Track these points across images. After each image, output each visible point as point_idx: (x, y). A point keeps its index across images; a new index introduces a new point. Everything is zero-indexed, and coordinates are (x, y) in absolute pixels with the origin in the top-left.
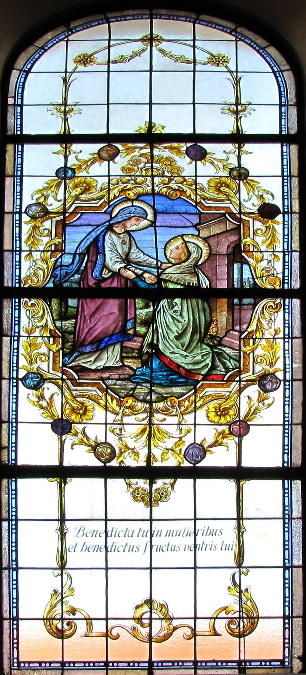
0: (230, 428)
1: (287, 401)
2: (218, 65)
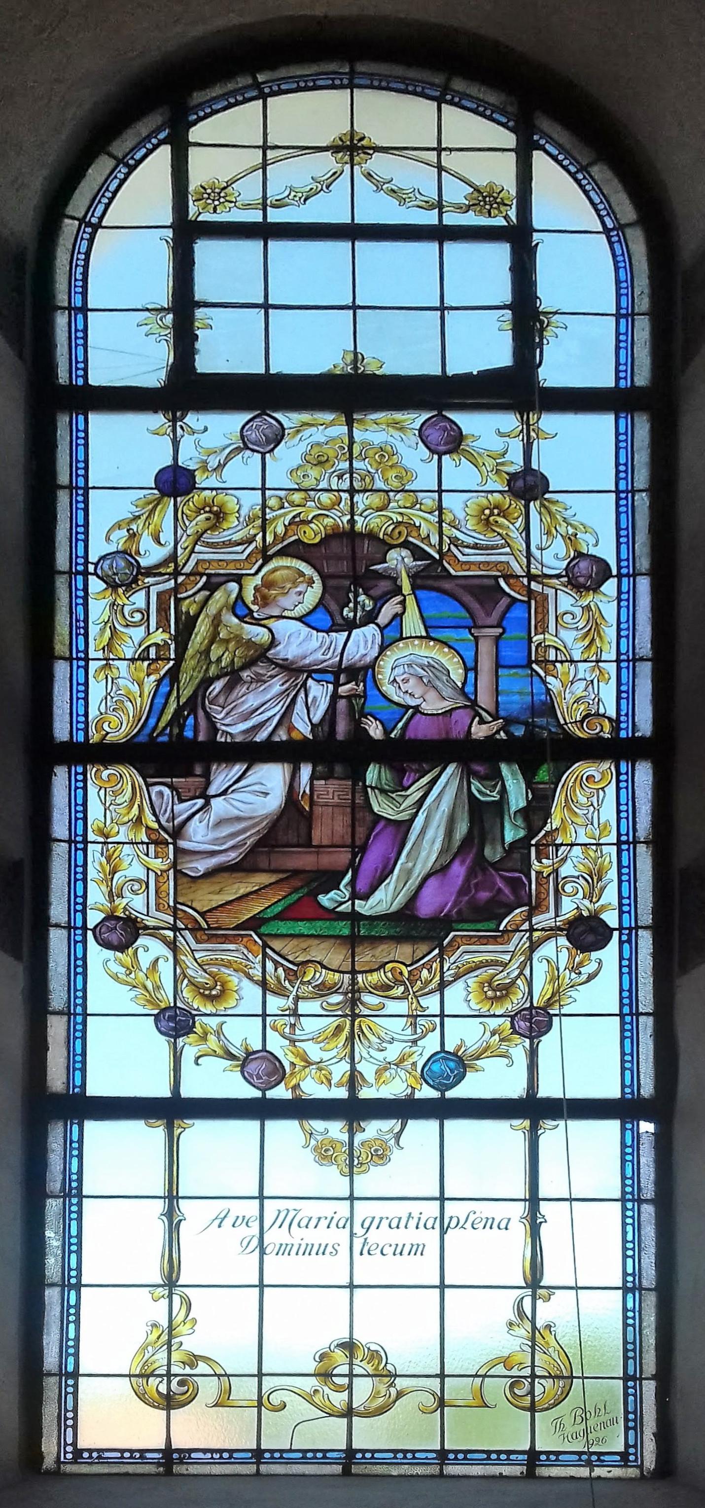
0: (512, 1023)
1: (628, 967)
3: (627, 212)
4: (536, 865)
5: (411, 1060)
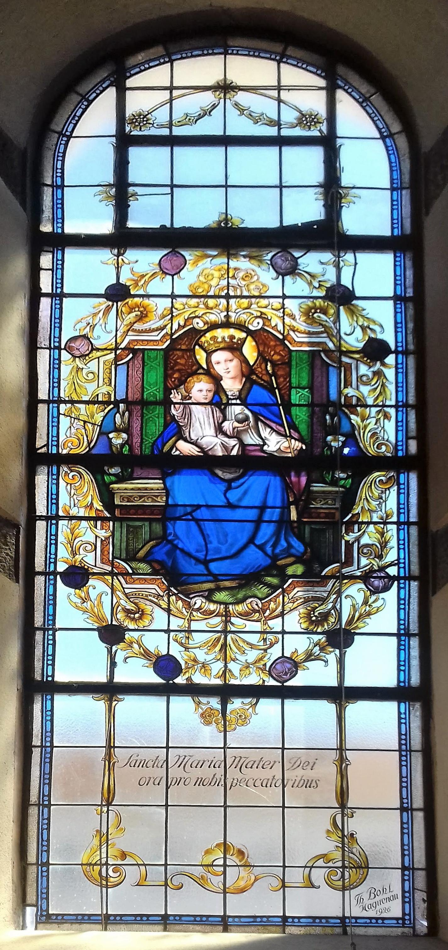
1: (402, 604)
2: (310, 128)
5: (262, 663)
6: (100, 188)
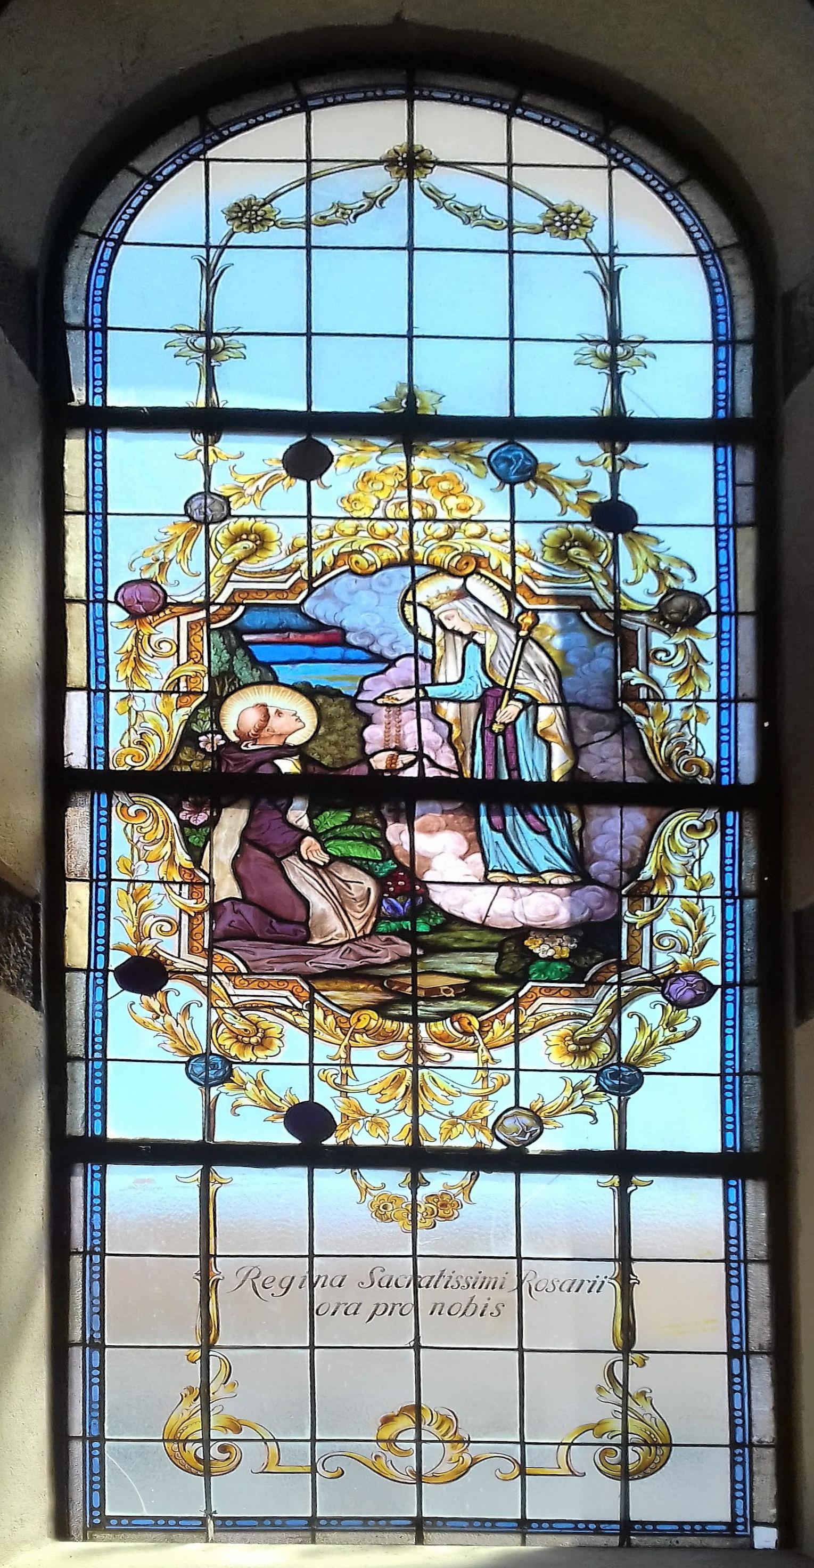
2: (567, 234)
3: (723, 233)
4: (629, 918)
6: (177, 335)
